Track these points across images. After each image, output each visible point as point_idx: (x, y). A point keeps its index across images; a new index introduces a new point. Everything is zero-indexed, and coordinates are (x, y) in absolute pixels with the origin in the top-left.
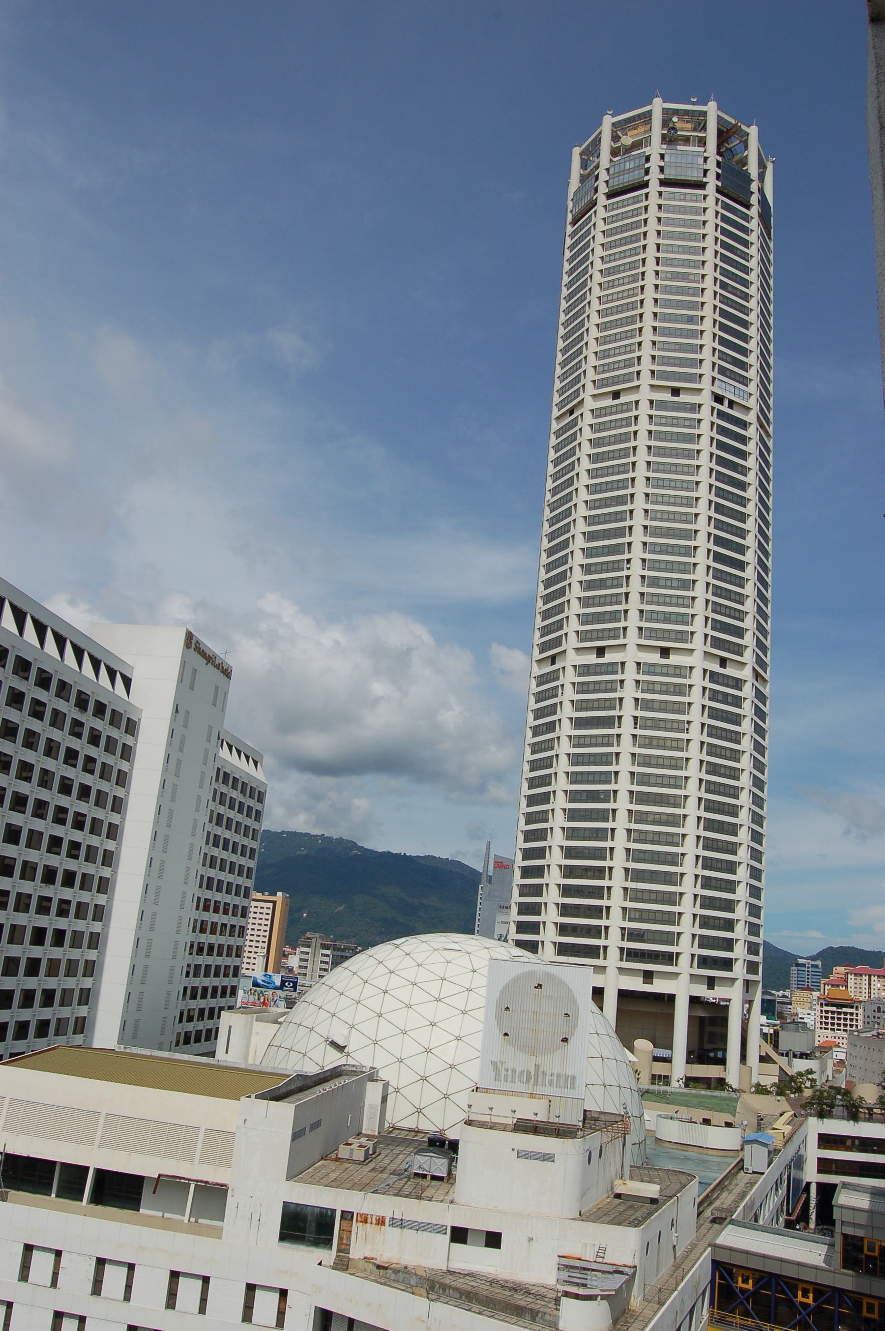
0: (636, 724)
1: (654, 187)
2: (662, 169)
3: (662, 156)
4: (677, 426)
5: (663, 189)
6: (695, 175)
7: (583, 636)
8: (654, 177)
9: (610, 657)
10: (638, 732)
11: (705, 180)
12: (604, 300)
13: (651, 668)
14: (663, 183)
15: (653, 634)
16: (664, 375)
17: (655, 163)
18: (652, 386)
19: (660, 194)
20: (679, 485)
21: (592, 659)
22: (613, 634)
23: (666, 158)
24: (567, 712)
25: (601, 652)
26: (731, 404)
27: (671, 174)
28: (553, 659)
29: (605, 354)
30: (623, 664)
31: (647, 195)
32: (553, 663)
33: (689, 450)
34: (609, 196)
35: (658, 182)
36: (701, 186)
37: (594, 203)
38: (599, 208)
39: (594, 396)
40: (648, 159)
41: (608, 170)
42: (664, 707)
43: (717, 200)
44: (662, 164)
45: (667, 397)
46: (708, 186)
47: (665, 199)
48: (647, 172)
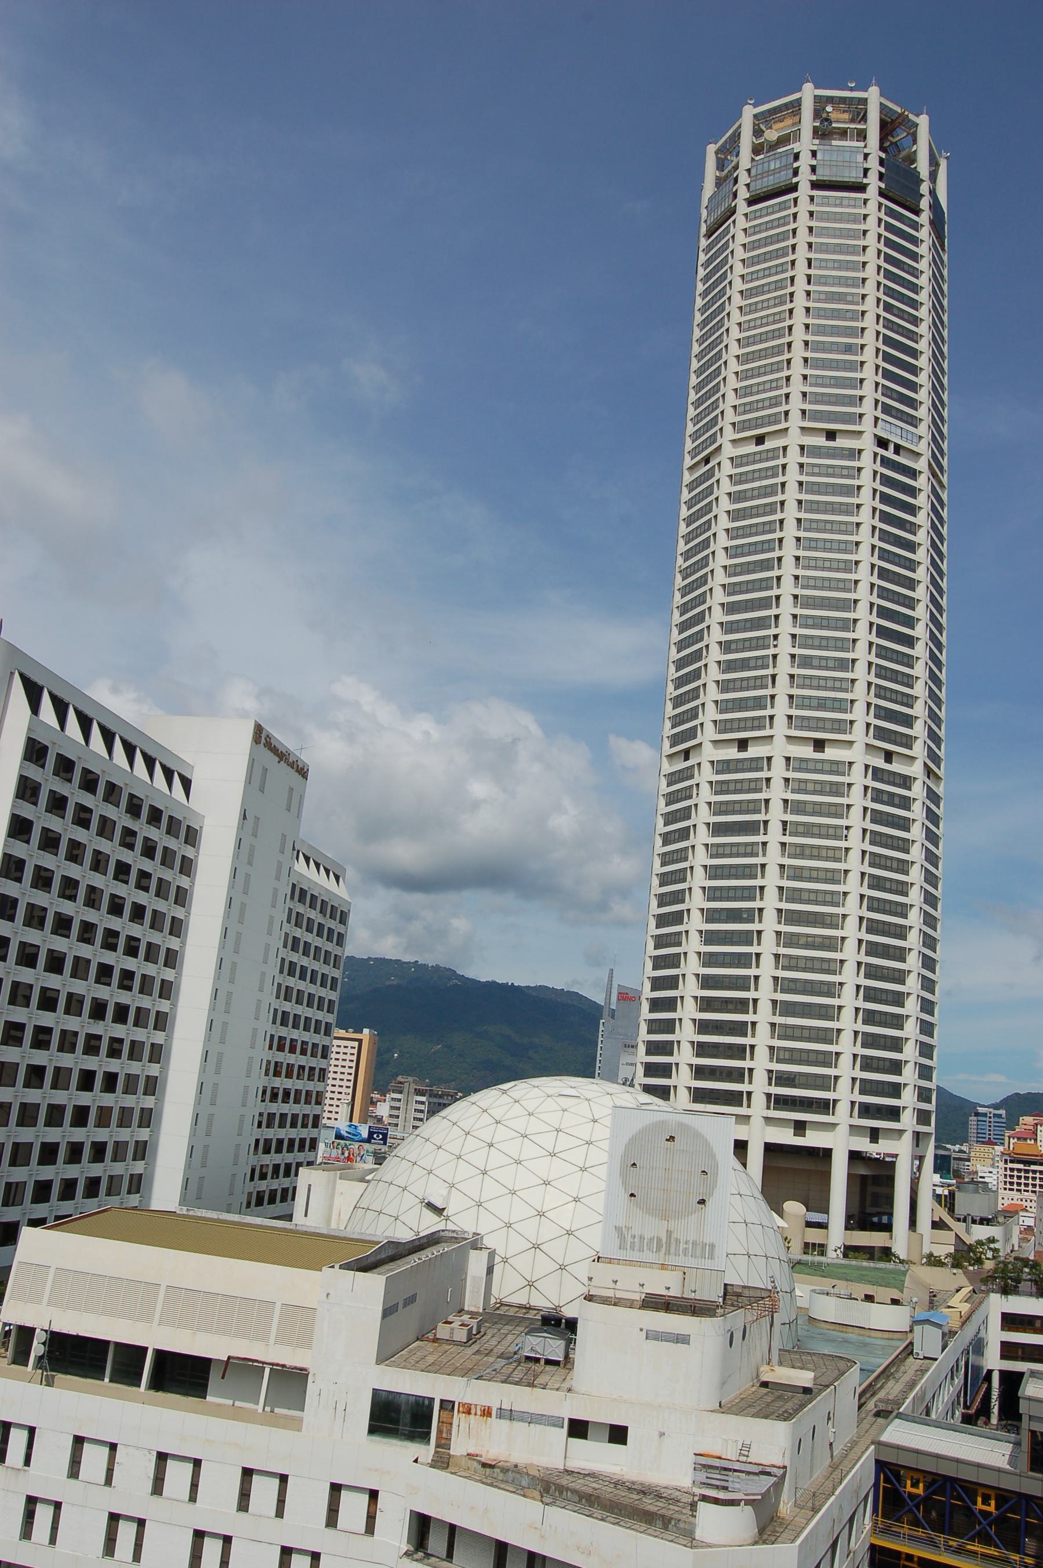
0: (785, 830)
1: (804, 190)
2: (813, 169)
3: (814, 154)
4: (833, 476)
5: (815, 193)
6: (853, 176)
7: (722, 726)
8: (804, 179)
9: (754, 751)
10: (787, 839)
11: (865, 181)
12: (745, 326)
13: (803, 764)
14: (815, 185)
15: (805, 723)
16: (817, 416)
17: (805, 162)
19: (812, 198)
20: (835, 546)
21: (732, 753)
22: (757, 723)
23: (819, 156)
24: (703, 816)
25: (743, 745)
26: (898, 449)
27: (824, 174)
28: (686, 754)
29: (747, 391)
30: (769, 759)
31: (796, 200)
32: (687, 758)
33: (847, 504)
34: (751, 202)
35: (809, 185)
36: (861, 188)
37: (733, 211)
38: (739, 217)
39: (734, 442)
40: (796, 157)
42: (818, 810)
43: (880, 205)
44: (814, 163)
45: (821, 441)
46: (869, 189)
47: (818, 205)
48: (796, 172)
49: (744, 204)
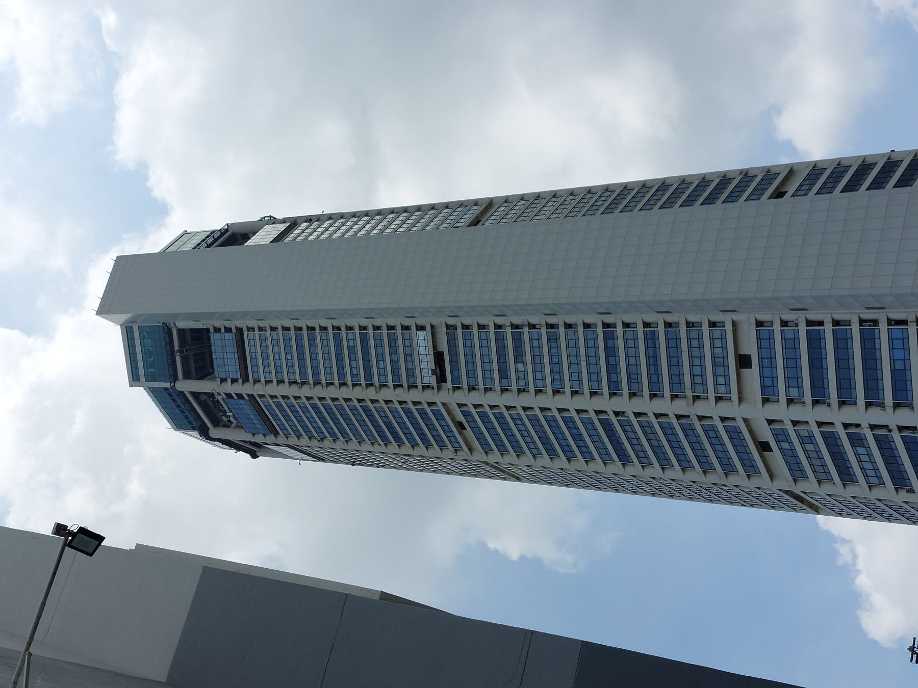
14: (246, 379)
18: (741, 400)
25: (764, 447)
40: (229, 396)
41: (264, 435)
46: (239, 326)
49: (445, 452)
